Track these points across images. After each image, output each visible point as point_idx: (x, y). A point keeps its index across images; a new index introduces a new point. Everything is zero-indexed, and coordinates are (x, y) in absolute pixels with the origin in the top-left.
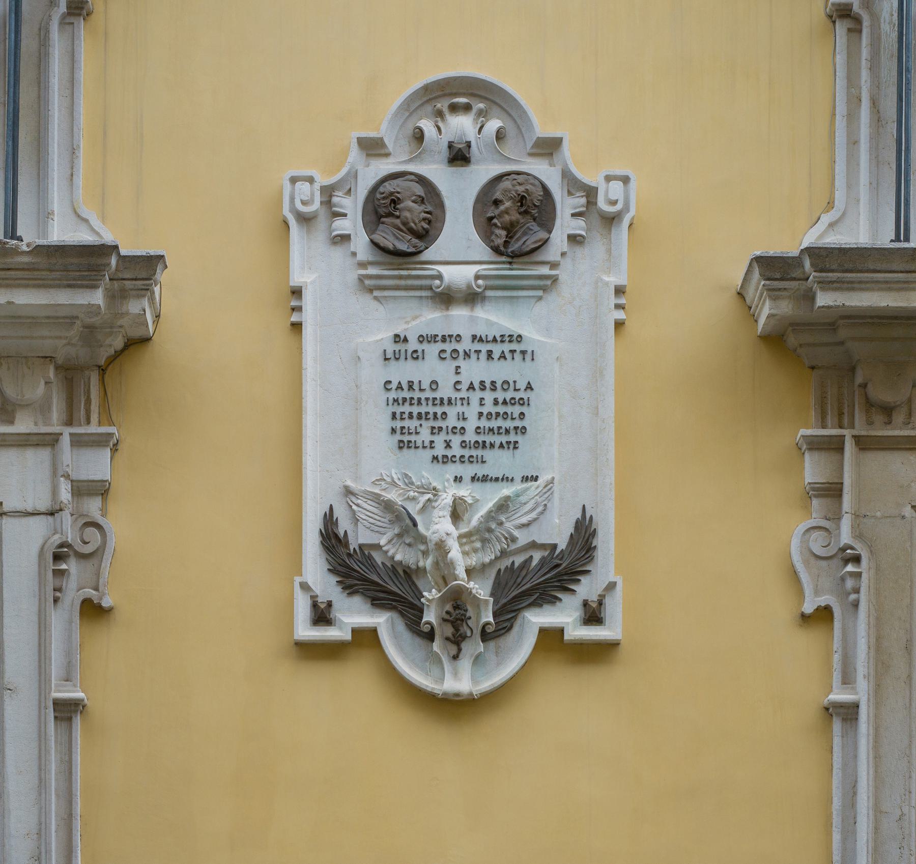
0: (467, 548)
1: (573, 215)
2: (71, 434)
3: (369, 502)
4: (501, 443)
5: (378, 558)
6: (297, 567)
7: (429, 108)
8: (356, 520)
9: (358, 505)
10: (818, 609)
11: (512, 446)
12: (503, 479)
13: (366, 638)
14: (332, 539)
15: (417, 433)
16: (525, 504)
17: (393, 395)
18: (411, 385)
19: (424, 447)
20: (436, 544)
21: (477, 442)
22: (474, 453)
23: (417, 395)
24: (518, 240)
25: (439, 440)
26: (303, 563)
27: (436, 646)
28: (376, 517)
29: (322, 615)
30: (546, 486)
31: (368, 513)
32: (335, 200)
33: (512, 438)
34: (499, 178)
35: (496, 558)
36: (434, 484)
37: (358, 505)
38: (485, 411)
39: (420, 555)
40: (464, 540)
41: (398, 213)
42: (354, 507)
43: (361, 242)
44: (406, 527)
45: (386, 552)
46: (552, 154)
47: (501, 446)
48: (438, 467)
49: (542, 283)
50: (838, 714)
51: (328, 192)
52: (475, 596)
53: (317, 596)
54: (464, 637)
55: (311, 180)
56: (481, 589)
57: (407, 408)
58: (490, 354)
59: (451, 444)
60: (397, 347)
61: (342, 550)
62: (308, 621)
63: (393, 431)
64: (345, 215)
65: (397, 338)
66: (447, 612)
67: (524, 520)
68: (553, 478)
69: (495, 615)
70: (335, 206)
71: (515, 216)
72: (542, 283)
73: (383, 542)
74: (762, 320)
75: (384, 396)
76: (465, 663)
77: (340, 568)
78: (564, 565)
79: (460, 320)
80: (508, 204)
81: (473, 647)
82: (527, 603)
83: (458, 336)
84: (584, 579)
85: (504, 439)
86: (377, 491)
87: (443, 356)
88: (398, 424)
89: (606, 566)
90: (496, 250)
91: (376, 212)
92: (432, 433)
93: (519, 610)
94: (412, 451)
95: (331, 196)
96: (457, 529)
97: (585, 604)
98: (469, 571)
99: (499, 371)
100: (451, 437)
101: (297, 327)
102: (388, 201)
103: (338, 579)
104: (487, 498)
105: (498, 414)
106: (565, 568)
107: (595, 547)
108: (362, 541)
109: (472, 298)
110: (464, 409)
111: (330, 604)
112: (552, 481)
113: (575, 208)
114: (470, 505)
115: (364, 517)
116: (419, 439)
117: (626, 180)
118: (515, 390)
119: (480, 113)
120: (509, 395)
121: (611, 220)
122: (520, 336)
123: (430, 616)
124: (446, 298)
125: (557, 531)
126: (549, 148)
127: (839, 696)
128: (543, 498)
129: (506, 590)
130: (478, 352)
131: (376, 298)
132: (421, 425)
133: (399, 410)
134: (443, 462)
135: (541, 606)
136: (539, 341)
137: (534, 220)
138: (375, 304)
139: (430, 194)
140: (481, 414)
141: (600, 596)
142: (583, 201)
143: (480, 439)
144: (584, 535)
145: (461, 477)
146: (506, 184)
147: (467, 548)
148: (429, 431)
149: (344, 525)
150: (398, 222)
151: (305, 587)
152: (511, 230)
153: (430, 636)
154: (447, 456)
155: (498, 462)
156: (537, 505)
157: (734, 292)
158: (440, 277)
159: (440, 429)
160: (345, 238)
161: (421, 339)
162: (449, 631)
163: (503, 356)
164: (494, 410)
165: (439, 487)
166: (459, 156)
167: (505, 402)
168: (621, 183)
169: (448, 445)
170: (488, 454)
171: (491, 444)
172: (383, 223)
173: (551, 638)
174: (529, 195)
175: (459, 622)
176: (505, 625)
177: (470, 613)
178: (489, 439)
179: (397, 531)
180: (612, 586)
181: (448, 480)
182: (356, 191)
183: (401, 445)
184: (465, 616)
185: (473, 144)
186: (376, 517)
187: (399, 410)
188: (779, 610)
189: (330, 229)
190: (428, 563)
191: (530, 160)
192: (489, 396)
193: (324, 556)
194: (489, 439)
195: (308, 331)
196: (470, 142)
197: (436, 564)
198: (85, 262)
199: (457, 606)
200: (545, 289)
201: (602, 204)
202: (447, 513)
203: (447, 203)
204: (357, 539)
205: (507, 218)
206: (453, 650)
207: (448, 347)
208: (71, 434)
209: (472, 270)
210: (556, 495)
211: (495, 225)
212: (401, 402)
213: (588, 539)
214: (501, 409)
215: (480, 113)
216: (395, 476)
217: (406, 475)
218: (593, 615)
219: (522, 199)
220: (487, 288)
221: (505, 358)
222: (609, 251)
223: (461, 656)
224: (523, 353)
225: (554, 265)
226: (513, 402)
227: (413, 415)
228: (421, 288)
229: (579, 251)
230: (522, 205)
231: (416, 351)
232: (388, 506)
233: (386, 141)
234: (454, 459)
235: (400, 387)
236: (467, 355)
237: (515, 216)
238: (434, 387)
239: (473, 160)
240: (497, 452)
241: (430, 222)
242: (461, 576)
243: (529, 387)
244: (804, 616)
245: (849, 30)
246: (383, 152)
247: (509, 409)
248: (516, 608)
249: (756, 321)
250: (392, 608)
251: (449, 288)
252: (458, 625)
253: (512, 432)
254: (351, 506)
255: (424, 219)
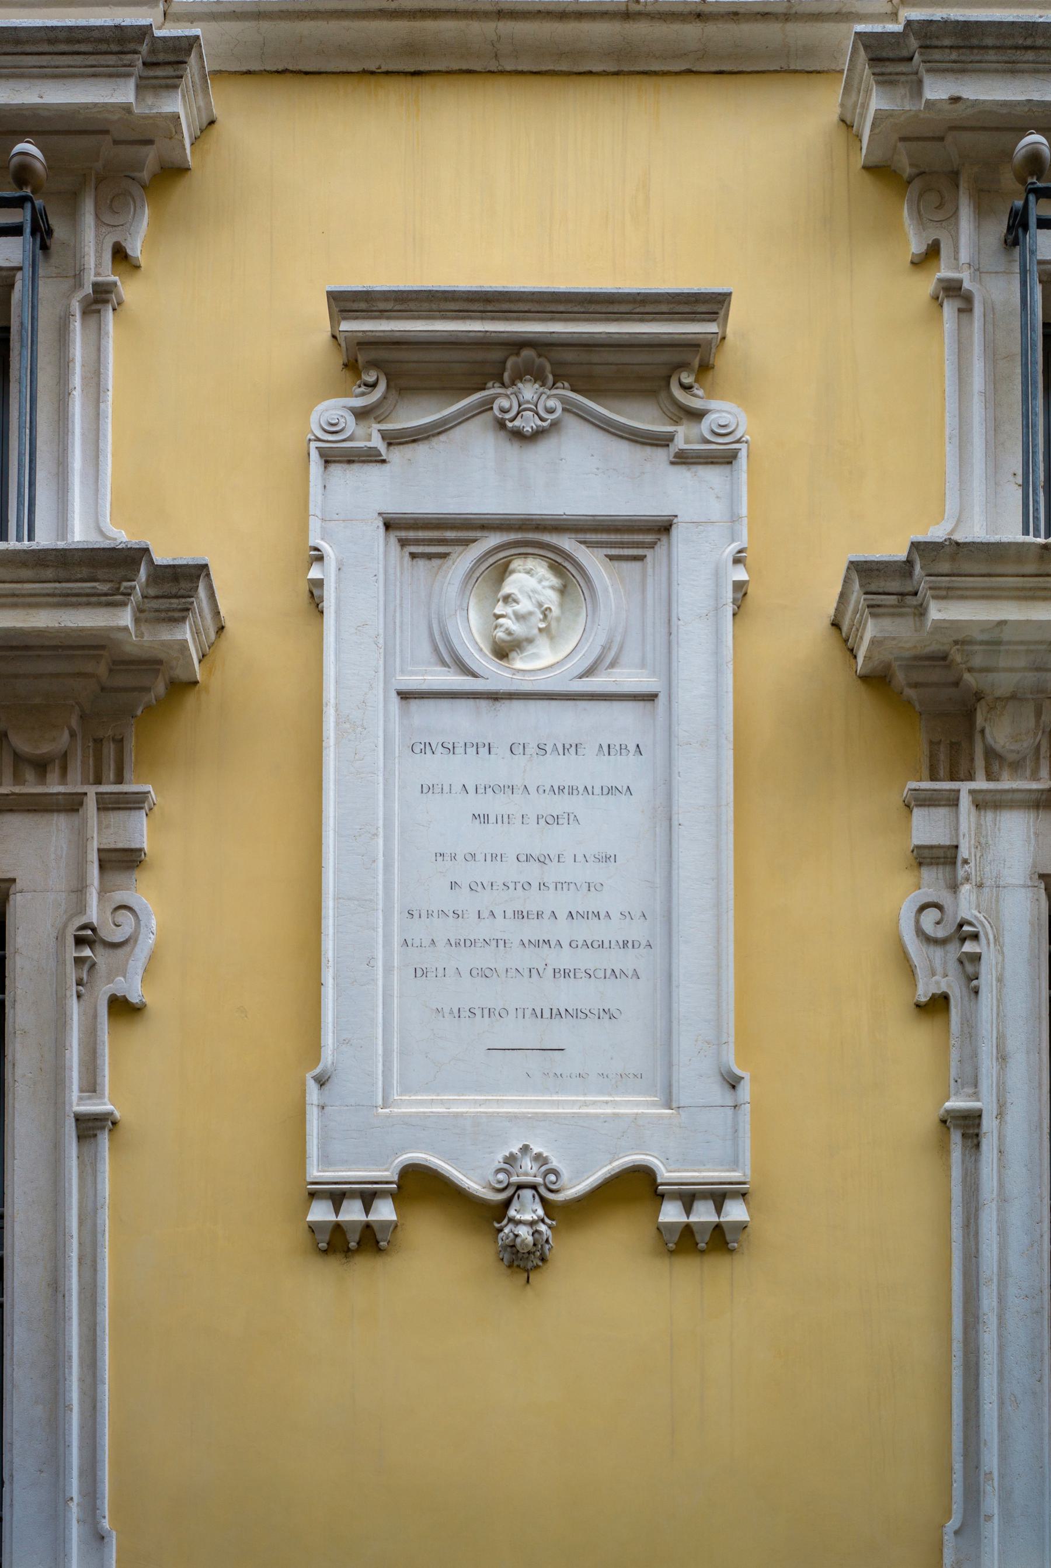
2: (97, 793)
10: (934, 998)
50: (956, 1126)
74: (860, 660)
127: (956, 1103)
157: (827, 622)
188: (895, 1002)
198: (109, 568)
208: (97, 793)
244: (918, 1005)
245: (960, 310)
249: (855, 657)
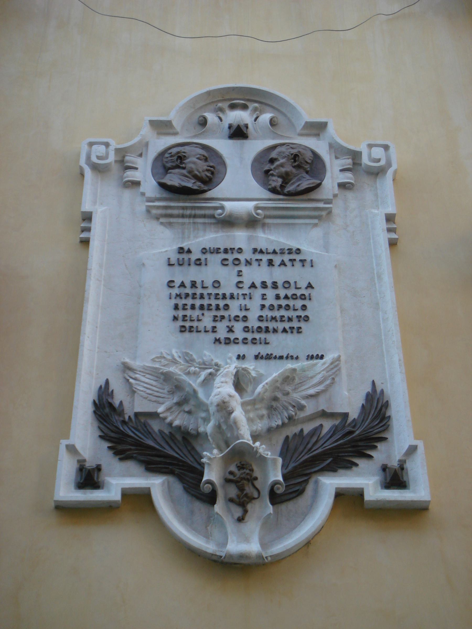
0: (251, 415)
1: (341, 171)
3: (147, 376)
4: (284, 328)
5: (155, 426)
6: (64, 428)
7: (212, 107)
8: (133, 392)
9: (135, 379)
11: (295, 331)
12: (287, 358)
13: (139, 501)
14: (105, 409)
15: (199, 320)
16: (312, 378)
17: (176, 291)
18: (194, 284)
19: (206, 331)
20: (218, 405)
21: (260, 327)
22: (257, 336)
23: (199, 291)
24: (293, 184)
25: (222, 327)
26: (73, 416)
27: (218, 508)
28: (154, 388)
29: (89, 478)
30: (332, 363)
31: (145, 385)
32: (127, 158)
33: (295, 324)
34: (273, 148)
35: (284, 424)
36: (216, 360)
37: (135, 379)
38: (267, 304)
39: (200, 421)
40: (249, 408)
41: (184, 165)
42: (131, 380)
43: (150, 186)
44: (186, 400)
45: (165, 419)
46: (318, 135)
47: (285, 331)
48: (223, 347)
49: (316, 213)
51: (122, 154)
52: (261, 456)
53: (85, 461)
54: (251, 499)
55: (107, 145)
56: (268, 451)
57: (189, 302)
58: (271, 263)
59: (233, 329)
60: (181, 256)
61: (116, 419)
62: (72, 486)
63: (175, 318)
64: (136, 169)
65: (181, 250)
66: (231, 473)
67: (312, 391)
68: (339, 357)
69: (284, 476)
70: (128, 162)
71: (288, 168)
72: (316, 213)
73: (160, 409)
75: (167, 291)
76: (253, 526)
77: (112, 435)
78: (357, 432)
79: (240, 238)
80: (282, 161)
81: (263, 508)
82: (322, 466)
83: (240, 249)
84: (380, 446)
85: (287, 325)
86: (157, 366)
87: (226, 263)
88: (181, 313)
89: (403, 433)
90: (274, 191)
91: (164, 167)
92: (215, 320)
93: (309, 475)
94: (194, 334)
95: (124, 157)
96: (241, 399)
97: (384, 468)
98: (255, 437)
99: (279, 275)
100: (233, 323)
101: (85, 242)
102: (175, 158)
103: (110, 445)
104: (272, 372)
105: (280, 307)
106: (359, 435)
107: (389, 417)
108: (138, 409)
109: (251, 222)
110: (247, 302)
111: (99, 468)
112: (338, 359)
113: (343, 166)
114: (254, 378)
115: (142, 389)
116: (201, 326)
117: (386, 147)
118: (296, 288)
119: (255, 109)
120: (290, 293)
121: (377, 173)
122: (298, 249)
123: (212, 475)
124: (229, 222)
125: (349, 401)
126: (317, 129)
128: (330, 373)
129: (296, 455)
130: (259, 260)
131: (162, 223)
132: (203, 314)
133: (181, 302)
134: (226, 343)
135: (335, 471)
136: (317, 253)
137: (307, 172)
138: (161, 228)
139: (213, 158)
140: (263, 306)
141: (400, 461)
142: (350, 161)
143: (263, 325)
144: (377, 410)
145: (244, 355)
146: (278, 149)
147: (251, 415)
148: (212, 319)
149: (120, 396)
150: (184, 172)
151: (72, 449)
152: (286, 178)
153: (210, 498)
154: (229, 339)
155: (280, 343)
156: (325, 379)
158: (222, 208)
159: (223, 317)
160: (136, 184)
161: (204, 251)
162: (233, 491)
163: (283, 264)
164: (276, 303)
165: (220, 362)
166: (238, 133)
167: (286, 297)
168: (382, 149)
169: (231, 330)
170: (271, 337)
171: (274, 329)
172: (170, 173)
173: (349, 501)
174: (300, 154)
175: (245, 482)
176: (297, 488)
177: (257, 473)
178: (272, 325)
179: (176, 399)
180: (412, 450)
181: (230, 358)
182: (146, 154)
183: (183, 329)
184: (251, 476)
185: (250, 126)
186: (154, 388)
187: (181, 302)
189: (122, 178)
190: (209, 428)
191: (299, 138)
192: (271, 293)
193: (96, 424)
194: (272, 325)
195: (95, 244)
196: (247, 124)
197: (218, 427)
199: (242, 469)
200: (319, 218)
201: (365, 160)
202: (230, 380)
203: (228, 161)
204: (133, 409)
205: (283, 170)
206: (238, 512)
207: (231, 257)
209: (250, 205)
210: (344, 372)
211: (272, 175)
212: (183, 297)
213: (381, 409)
214: (283, 303)
215: (255, 109)
216: (175, 355)
217: (187, 354)
218: (395, 478)
219: (295, 157)
220: (266, 217)
221: (285, 265)
222: (376, 195)
223: (247, 518)
224: (303, 261)
225: (328, 202)
226: (294, 297)
227: (193, 307)
228: (204, 216)
229: (349, 195)
230: (295, 161)
231: (199, 260)
232: (167, 377)
233: (174, 123)
234: (237, 341)
235: (182, 285)
236: (248, 263)
237: (288, 168)
238: (216, 285)
239: (250, 136)
240: (281, 337)
241: (213, 173)
242: (245, 436)
243: (310, 286)
246: (171, 131)
247: (291, 303)
248: (308, 471)
250: (170, 472)
251: (230, 216)
252: (243, 485)
253: (295, 320)
254: (128, 380)
255: (208, 170)
